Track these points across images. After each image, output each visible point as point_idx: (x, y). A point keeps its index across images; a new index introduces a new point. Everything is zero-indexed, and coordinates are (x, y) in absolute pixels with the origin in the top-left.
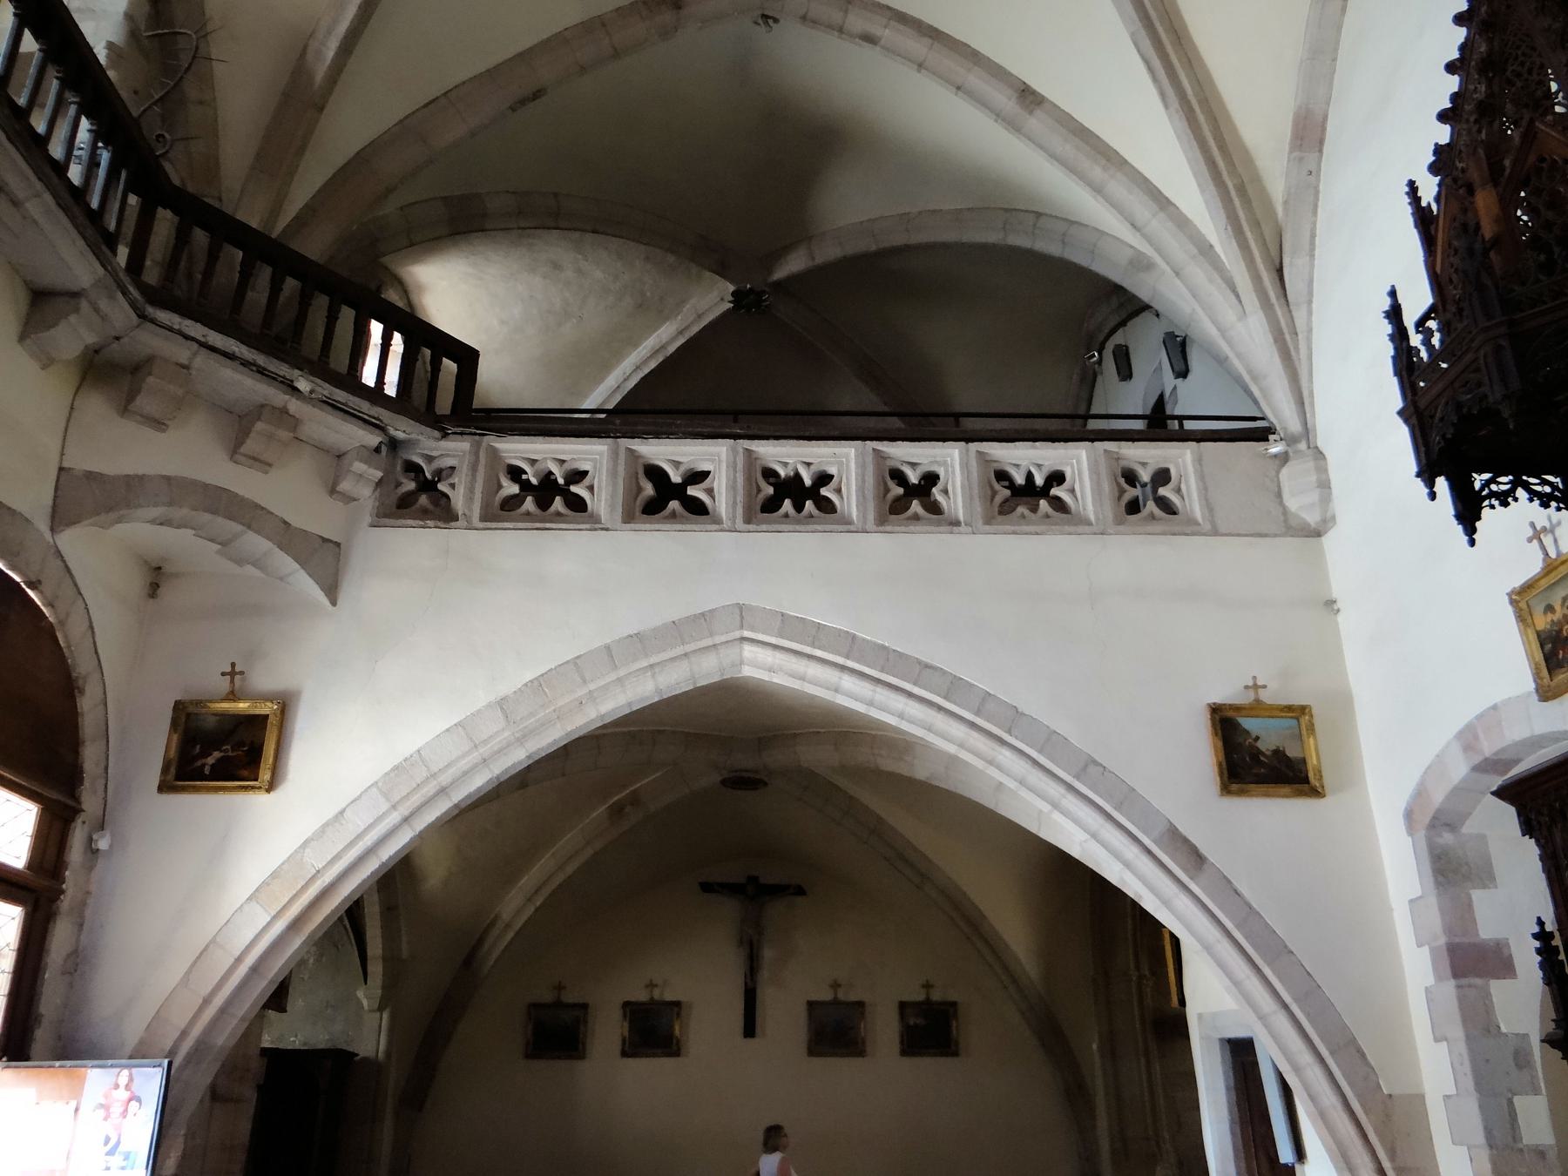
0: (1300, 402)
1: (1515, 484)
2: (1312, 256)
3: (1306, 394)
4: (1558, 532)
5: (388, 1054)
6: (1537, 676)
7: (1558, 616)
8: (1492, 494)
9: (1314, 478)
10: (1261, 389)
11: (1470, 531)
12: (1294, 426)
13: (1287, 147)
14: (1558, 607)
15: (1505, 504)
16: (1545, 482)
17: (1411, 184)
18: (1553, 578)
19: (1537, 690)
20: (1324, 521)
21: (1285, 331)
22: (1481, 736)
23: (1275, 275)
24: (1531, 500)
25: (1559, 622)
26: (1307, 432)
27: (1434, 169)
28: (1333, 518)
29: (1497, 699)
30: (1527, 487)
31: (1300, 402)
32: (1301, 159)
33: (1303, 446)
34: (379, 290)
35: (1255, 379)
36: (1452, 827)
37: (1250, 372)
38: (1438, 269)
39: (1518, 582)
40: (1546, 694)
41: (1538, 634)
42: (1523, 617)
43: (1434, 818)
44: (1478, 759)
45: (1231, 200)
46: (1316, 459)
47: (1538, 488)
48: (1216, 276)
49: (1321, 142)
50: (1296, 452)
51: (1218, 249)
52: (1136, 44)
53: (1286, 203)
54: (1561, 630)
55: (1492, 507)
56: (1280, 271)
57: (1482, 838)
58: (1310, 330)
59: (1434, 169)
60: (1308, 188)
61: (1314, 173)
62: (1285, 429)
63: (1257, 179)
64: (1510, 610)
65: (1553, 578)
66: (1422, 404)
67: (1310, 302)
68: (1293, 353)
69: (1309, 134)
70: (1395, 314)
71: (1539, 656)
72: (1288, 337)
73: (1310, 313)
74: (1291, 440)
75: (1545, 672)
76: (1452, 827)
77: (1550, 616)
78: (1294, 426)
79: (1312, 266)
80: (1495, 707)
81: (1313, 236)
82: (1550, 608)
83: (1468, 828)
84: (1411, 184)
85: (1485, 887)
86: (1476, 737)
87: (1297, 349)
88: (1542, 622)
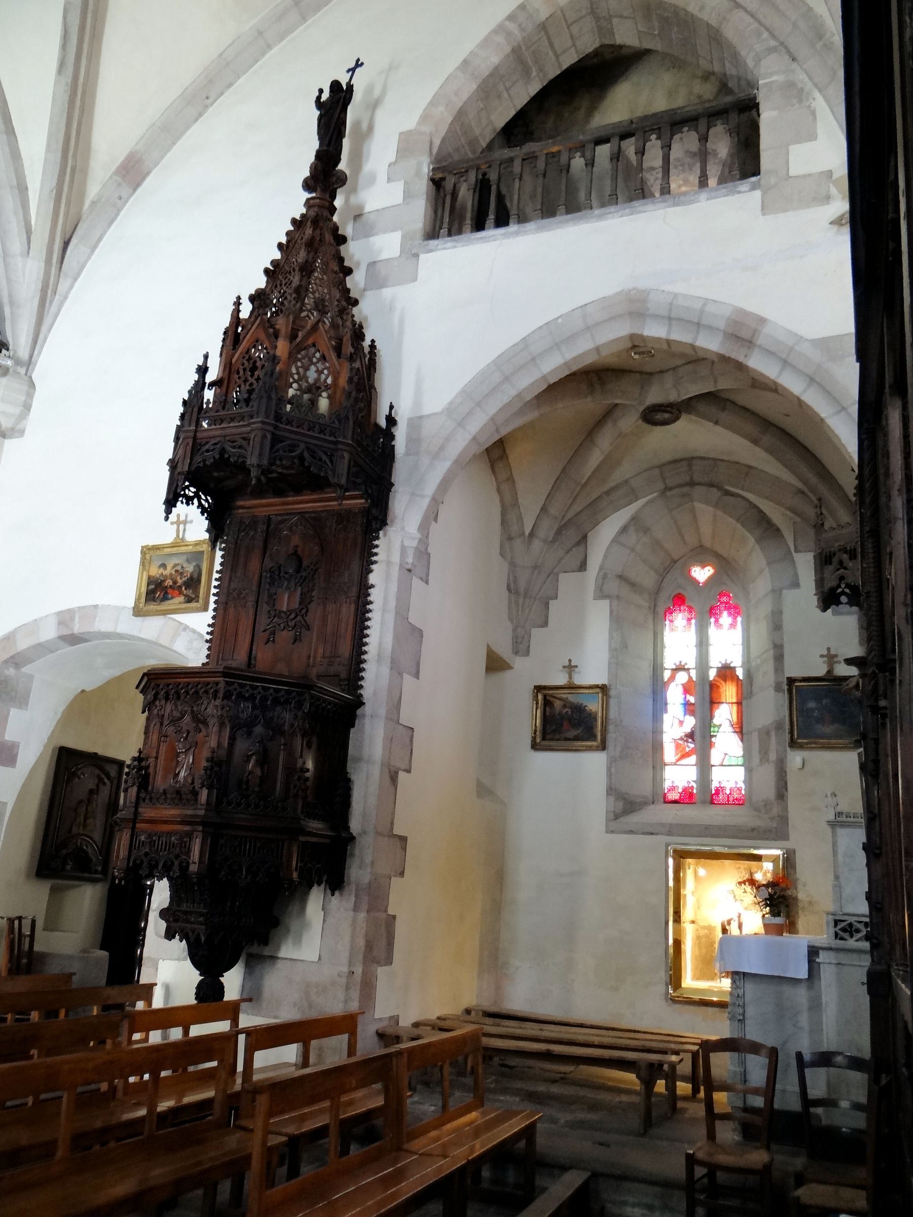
0: (35, 341)
1: (196, 495)
2: (93, 251)
3: (41, 337)
4: (188, 526)
5: (781, 849)
6: (137, 600)
7: (167, 572)
8: (185, 496)
9: (23, 398)
10: (12, 313)
11: (168, 512)
12: (23, 353)
13: (114, 168)
14: (169, 567)
15: (188, 504)
16: (207, 500)
17: (239, 298)
18: (174, 550)
19: (134, 608)
20: (13, 429)
21: (51, 287)
22: (77, 619)
23: (62, 245)
24: (198, 507)
25: (166, 576)
26: (29, 363)
27: (252, 299)
28: (22, 433)
29: (100, 603)
30: (199, 499)
31: (35, 341)
32: (119, 185)
33: (22, 371)
34: (734, 610)
35: (12, 303)
36: (17, 666)
37: (10, 296)
38: (234, 361)
39: (151, 543)
40: (138, 612)
41: (149, 577)
42: (144, 563)
43: (12, 657)
44: (66, 632)
45: (65, 174)
46: (29, 386)
47: (203, 502)
48: (21, 212)
49: (138, 185)
50: (15, 372)
51: (31, 193)
52: (66, 11)
53: (94, 203)
54: (164, 581)
55: (182, 503)
56: (66, 244)
57: (31, 677)
58: (66, 298)
59: (252, 299)
60: (112, 208)
61: (123, 200)
62: (15, 352)
63: (85, 172)
64: (139, 556)
65: (174, 550)
66: (199, 435)
67: (75, 279)
68: (47, 305)
69: (133, 172)
70: (202, 370)
71: (144, 589)
72: (49, 292)
73: (72, 287)
74: (18, 362)
75: (143, 600)
76: (17, 666)
77: (161, 570)
78: (23, 353)
79: (89, 258)
80: (96, 607)
81: (100, 240)
82: (163, 566)
83: (26, 669)
84: (239, 298)
85: (20, 708)
86: (72, 619)
87: (51, 302)
88: (155, 571)
